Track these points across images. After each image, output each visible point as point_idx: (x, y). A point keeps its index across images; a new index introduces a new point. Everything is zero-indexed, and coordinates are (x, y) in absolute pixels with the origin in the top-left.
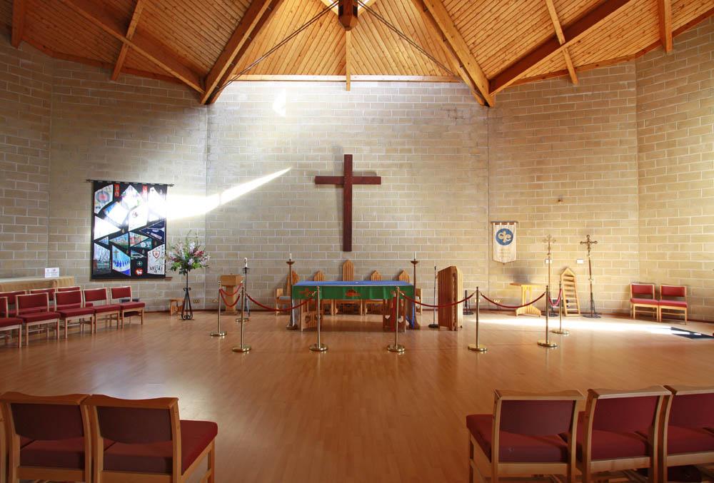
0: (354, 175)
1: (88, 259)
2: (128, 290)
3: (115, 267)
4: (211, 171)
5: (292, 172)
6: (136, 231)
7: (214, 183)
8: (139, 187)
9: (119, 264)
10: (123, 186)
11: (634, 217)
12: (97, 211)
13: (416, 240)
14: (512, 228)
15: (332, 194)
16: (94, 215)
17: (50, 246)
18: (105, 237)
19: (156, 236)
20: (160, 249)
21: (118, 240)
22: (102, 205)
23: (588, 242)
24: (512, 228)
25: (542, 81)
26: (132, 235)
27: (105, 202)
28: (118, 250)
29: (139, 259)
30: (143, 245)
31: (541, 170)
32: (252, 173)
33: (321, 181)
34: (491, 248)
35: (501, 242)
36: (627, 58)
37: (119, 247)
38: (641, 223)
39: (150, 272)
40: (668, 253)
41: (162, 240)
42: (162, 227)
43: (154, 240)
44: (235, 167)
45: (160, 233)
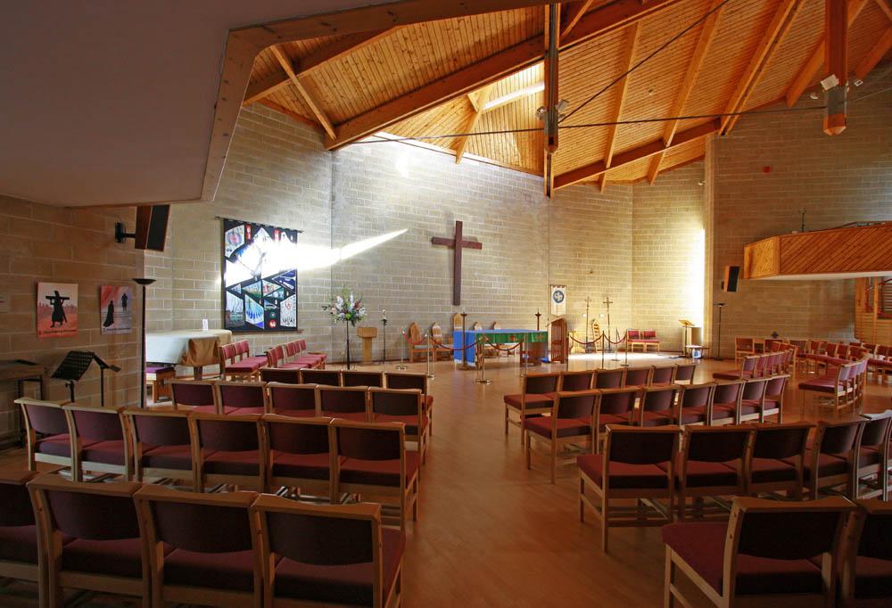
0: (463, 239)
1: (218, 310)
2: (246, 345)
3: (248, 319)
4: (336, 220)
5: (408, 232)
6: (269, 279)
7: (339, 235)
8: (271, 231)
9: (252, 316)
10: (255, 228)
11: (629, 287)
12: (228, 254)
13: (505, 297)
14: (563, 290)
15: (445, 253)
16: (224, 259)
17: (174, 293)
18: (235, 285)
19: (288, 285)
20: (291, 300)
21: (251, 289)
22: (234, 248)
23: (608, 303)
24: (563, 290)
25: (583, 186)
26: (265, 283)
27: (236, 245)
28: (251, 300)
29: (272, 310)
30: (276, 295)
31: (581, 250)
32: (377, 228)
33: (436, 241)
34: (550, 305)
35: (556, 300)
36: (629, 182)
37: (251, 295)
38: (633, 290)
39: (282, 324)
40: (647, 310)
41: (294, 290)
42: (293, 276)
43: (286, 289)
44: (360, 219)
45: (292, 282)
